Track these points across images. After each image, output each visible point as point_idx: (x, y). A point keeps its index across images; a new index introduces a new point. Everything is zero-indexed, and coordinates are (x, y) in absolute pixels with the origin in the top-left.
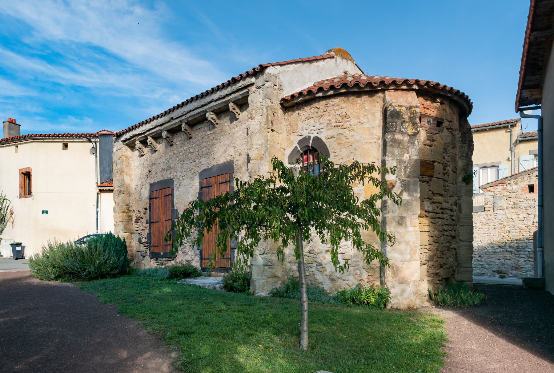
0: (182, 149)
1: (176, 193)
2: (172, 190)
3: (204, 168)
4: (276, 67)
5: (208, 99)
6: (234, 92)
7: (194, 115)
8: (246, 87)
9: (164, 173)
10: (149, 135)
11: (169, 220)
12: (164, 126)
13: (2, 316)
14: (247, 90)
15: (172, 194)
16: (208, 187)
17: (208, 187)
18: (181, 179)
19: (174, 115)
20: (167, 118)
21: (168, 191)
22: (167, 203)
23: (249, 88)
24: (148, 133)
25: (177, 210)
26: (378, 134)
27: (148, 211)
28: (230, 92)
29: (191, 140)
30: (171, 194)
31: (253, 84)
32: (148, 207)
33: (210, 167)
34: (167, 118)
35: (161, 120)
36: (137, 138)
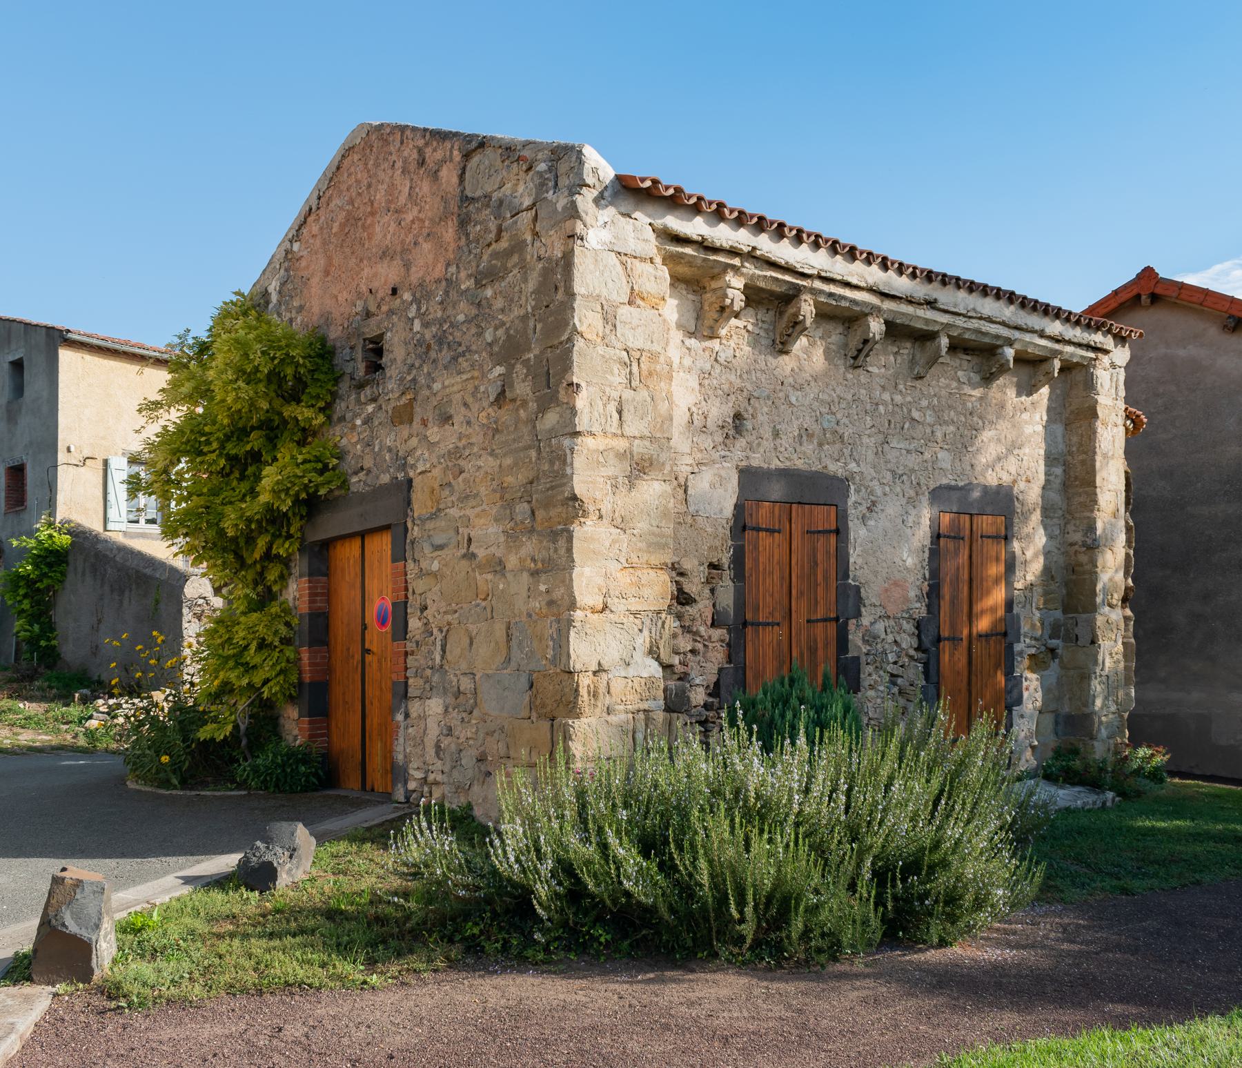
0: (886, 396)
1: (858, 533)
2: (842, 517)
3: (945, 481)
4: (839, 278)
5: (1035, 321)
6: (1079, 345)
7: (986, 334)
8: (1096, 349)
9: (809, 448)
10: (813, 291)
11: (825, 620)
12: (888, 305)
13: (1239, 839)
14: (1092, 355)
15: (840, 531)
16: (954, 538)
17: (954, 538)
18: (879, 492)
19: (946, 297)
20: (919, 289)
21: (823, 517)
22: (820, 557)
23: (1100, 355)
24: (818, 284)
25: (858, 589)
26: (863, 532)
27: (727, 574)
28: (1075, 340)
29: (918, 384)
30: (837, 532)
31: (1106, 352)
32: (726, 559)
33: (961, 484)
34: (919, 289)
35: (902, 284)
36: (750, 268)
